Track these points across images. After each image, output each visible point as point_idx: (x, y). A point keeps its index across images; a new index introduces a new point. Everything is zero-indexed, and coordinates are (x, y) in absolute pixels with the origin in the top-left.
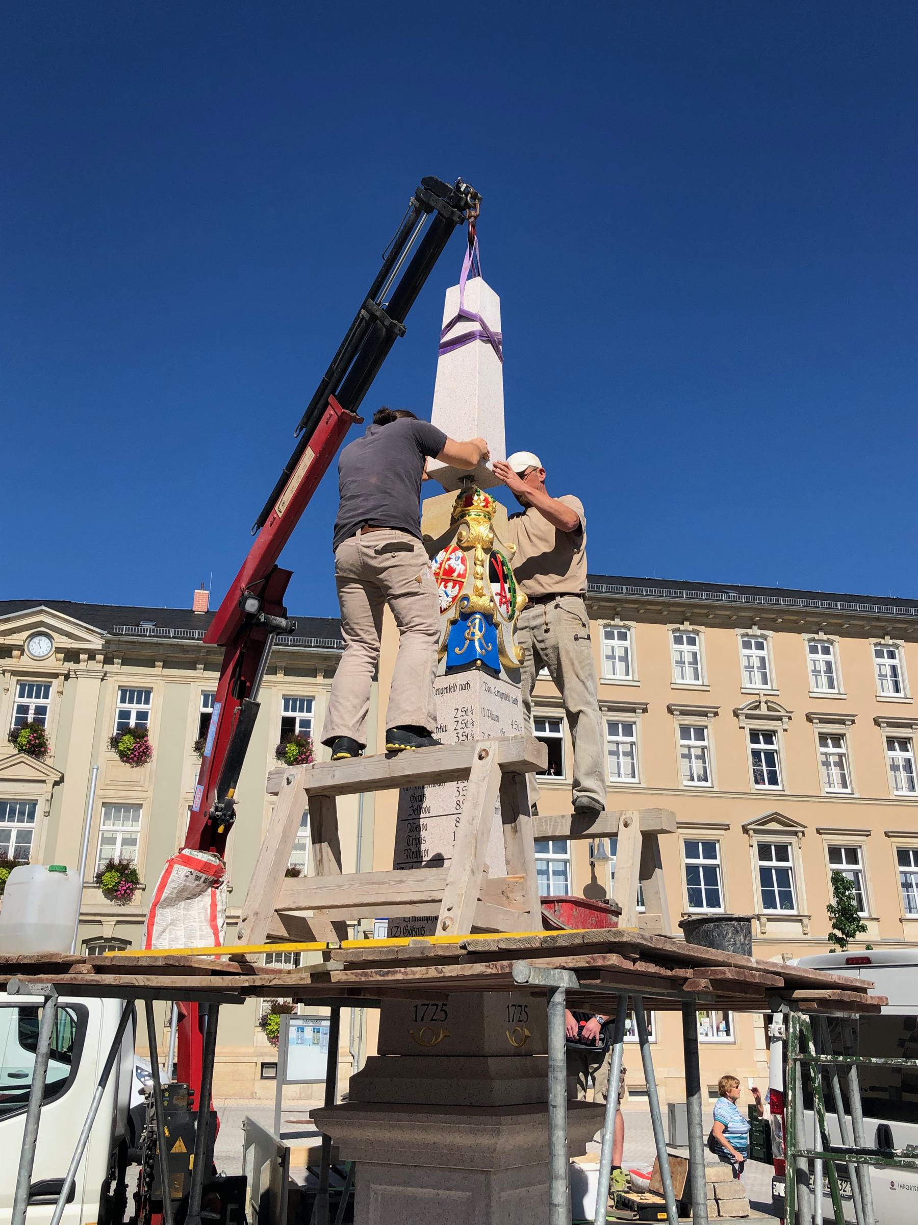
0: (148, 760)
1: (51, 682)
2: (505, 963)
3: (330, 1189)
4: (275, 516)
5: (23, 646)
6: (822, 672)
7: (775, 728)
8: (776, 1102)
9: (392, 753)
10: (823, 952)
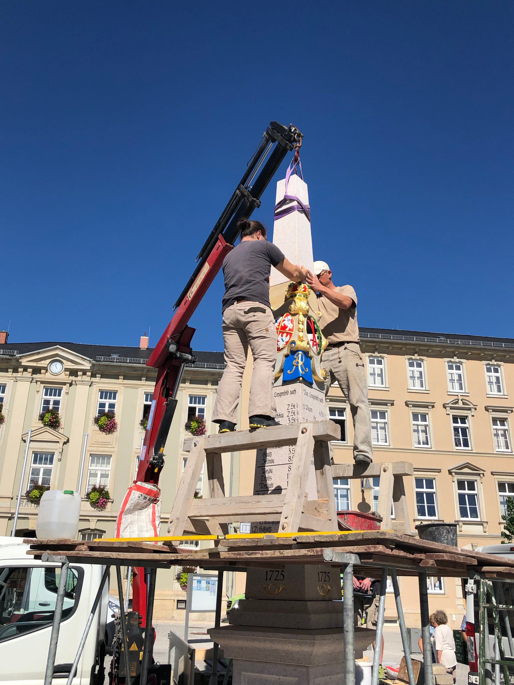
0: (115, 431)
1: (62, 387)
2: (319, 549)
3: (218, 673)
4: (187, 299)
5: (47, 367)
6: (494, 383)
7: (467, 415)
8: (470, 630)
9: (253, 429)
10: (497, 543)
